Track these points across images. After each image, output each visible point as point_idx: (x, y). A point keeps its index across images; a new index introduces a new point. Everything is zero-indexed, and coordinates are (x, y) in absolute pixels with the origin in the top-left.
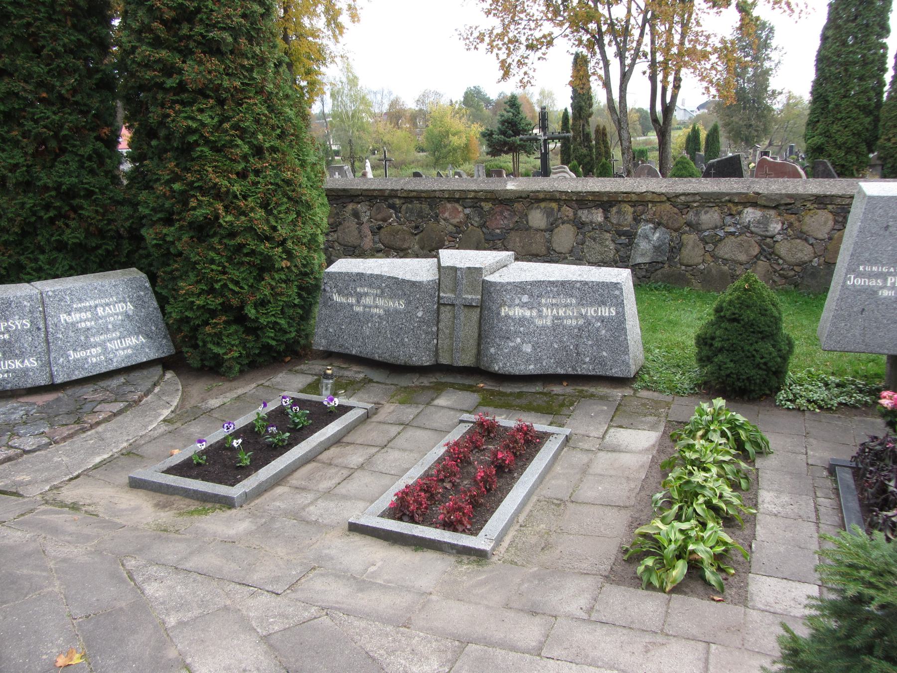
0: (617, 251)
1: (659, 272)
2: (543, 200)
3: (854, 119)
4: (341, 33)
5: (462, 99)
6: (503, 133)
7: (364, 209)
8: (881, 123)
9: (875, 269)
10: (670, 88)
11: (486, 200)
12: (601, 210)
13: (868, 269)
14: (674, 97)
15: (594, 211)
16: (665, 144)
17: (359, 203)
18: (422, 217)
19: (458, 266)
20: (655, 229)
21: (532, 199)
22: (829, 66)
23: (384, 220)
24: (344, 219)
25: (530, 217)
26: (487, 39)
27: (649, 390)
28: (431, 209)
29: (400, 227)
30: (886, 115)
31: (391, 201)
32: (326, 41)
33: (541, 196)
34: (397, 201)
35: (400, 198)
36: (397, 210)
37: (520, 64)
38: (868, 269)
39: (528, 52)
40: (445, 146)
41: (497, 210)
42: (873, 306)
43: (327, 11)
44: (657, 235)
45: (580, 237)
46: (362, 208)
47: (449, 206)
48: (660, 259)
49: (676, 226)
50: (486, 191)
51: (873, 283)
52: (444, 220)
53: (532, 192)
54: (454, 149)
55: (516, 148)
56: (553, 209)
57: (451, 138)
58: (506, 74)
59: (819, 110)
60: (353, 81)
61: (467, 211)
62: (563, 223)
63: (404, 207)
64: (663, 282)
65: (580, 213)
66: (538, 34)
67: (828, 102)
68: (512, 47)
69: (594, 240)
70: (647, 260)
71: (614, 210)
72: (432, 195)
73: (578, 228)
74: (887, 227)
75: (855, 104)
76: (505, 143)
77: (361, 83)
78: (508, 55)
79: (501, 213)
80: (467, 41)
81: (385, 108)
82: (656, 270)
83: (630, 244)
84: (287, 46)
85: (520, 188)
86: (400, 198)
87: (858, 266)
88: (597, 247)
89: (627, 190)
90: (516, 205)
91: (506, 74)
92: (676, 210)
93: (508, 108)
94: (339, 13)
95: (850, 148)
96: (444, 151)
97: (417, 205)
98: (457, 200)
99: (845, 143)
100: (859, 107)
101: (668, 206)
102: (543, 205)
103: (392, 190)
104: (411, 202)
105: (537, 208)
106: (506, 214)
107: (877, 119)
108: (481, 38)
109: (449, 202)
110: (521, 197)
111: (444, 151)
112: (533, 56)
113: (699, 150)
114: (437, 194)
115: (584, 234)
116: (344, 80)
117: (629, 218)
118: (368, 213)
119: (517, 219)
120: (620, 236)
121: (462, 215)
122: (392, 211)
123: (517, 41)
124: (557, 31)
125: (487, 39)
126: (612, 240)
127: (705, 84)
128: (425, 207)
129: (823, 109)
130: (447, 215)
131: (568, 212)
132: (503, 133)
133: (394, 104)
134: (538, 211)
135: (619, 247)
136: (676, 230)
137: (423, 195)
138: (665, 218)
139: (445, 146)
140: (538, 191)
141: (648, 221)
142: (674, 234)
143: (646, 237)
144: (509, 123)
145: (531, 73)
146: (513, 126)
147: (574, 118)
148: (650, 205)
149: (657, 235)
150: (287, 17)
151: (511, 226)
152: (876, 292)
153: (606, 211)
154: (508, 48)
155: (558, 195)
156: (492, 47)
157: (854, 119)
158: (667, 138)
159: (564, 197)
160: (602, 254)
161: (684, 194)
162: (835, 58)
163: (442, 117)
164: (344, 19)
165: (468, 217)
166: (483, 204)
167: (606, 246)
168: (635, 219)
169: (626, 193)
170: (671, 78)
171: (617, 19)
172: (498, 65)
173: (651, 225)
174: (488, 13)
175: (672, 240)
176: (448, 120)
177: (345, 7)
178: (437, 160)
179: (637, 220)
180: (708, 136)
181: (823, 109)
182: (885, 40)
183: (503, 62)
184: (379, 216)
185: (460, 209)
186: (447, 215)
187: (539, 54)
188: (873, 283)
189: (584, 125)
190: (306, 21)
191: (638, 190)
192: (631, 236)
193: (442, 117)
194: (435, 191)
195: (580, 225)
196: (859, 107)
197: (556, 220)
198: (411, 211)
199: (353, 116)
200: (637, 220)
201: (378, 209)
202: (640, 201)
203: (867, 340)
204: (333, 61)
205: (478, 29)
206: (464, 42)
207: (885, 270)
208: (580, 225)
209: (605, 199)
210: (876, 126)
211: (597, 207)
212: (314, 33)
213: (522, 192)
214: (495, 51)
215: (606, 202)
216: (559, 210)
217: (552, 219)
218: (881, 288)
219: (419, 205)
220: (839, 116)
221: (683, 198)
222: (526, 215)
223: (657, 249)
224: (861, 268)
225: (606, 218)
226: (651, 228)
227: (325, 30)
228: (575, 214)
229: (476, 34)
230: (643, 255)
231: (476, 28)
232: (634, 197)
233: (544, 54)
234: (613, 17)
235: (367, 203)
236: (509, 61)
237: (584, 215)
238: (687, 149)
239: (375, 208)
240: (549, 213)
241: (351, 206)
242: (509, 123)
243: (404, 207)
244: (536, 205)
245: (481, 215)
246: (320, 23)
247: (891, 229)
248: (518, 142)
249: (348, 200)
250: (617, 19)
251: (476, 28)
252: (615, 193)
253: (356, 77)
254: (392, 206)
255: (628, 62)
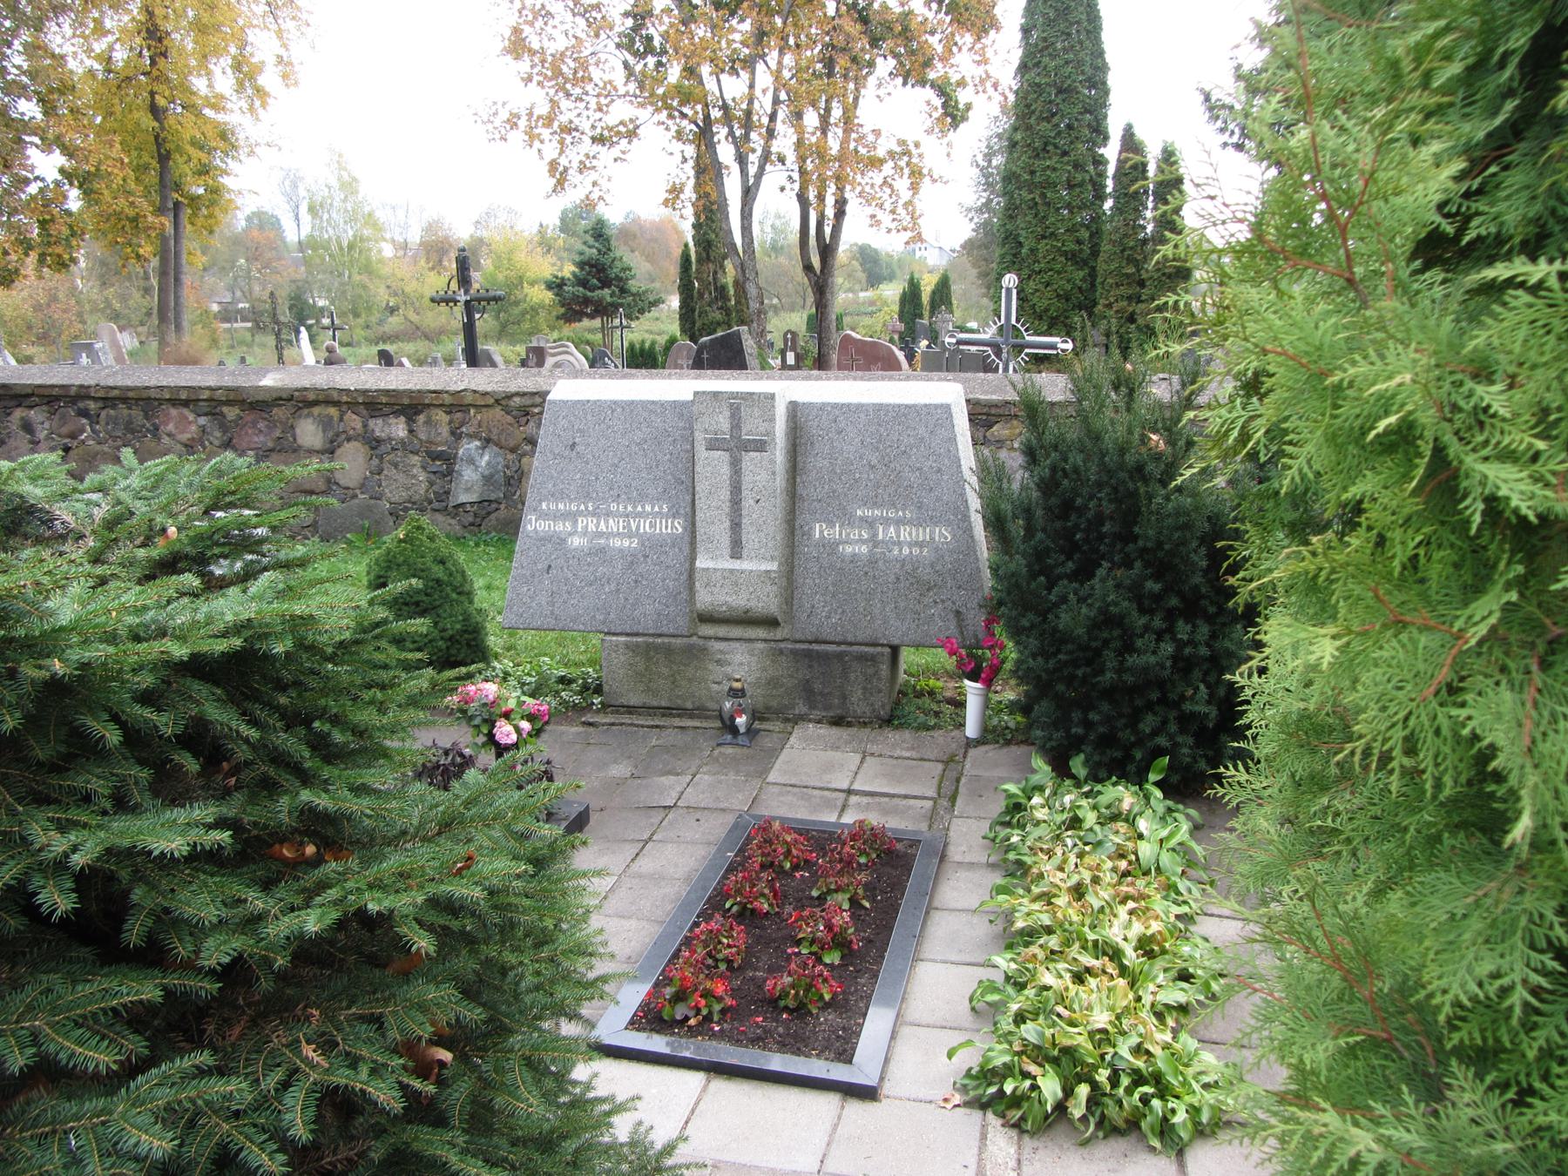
0: (432, 484)
1: (493, 516)
2: (316, 403)
3: (1059, 273)
4: (264, 105)
5: (558, 223)
6: (582, 283)
7: (40, 418)
8: (1099, 280)
9: (561, 506)
10: (830, 212)
11: (229, 403)
12: (402, 419)
13: (553, 507)
14: (837, 229)
15: (392, 420)
16: (826, 306)
17: (31, 407)
18: (133, 431)
19: (728, 524)
20: (484, 448)
21: (301, 401)
22: (1020, 188)
23: (73, 436)
24: (9, 435)
25: (298, 431)
26: (523, 123)
27: (849, 725)
28: (147, 417)
29: (98, 447)
30: (1105, 267)
31: (81, 405)
32: (235, 116)
33: (311, 397)
34: (92, 405)
35: (94, 399)
36: (94, 419)
37: (583, 168)
38: (553, 507)
39: (597, 148)
40: (517, 303)
41: (249, 418)
42: (561, 561)
43: (237, 66)
44: (486, 458)
45: (375, 462)
46: (36, 415)
47: (174, 412)
48: (493, 497)
49: (512, 443)
50: (228, 389)
51: (560, 527)
52: (169, 435)
53: (297, 390)
54: (532, 308)
55: (605, 308)
56: (331, 418)
57: (527, 288)
58: (561, 183)
59: (1009, 258)
60: (349, 187)
61: (202, 421)
62: (349, 440)
63: (103, 414)
64: (499, 531)
65: (372, 423)
66: (612, 119)
67: (1020, 244)
68: (569, 139)
69: (396, 466)
70: (473, 498)
71: (421, 418)
72: (145, 395)
73: (373, 448)
74: (574, 445)
75: (1059, 249)
76: (587, 301)
77: (365, 190)
78: (562, 152)
79: (254, 424)
80: (490, 127)
81: (415, 236)
82: (489, 513)
83: (449, 473)
84: (156, 124)
85: (279, 384)
86: (94, 399)
87: (540, 501)
88: (401, 477)
89: (438, 388)
90: (275, 410)
91: (561, 183)
92: (509, 419)
93: (591, 241)
94: (259, 69)
95: (1057, 318)
96: (516, 311)
97: (123, 411)
98: (186, 403)
99: (1046, 310)
100: (1065, 254)
101: (497, 412)
102: (316, 410)
103: (81, 386)
104: (114, 407)
105: (308, 416)
106: (261, 425)
107: (1093, 274)
108: (512, 122)
109: (174, 405)
110: (281, 399)
111: (516, 311)
112: (605, 154)
113: (921, 316)
114: (153, 393)
115: (381, 458)
116: (335, 183)
117: (445, 431)
118: (47, 425)
119: (278, 433)
120: (433, 460)
121: (193, 428)
122: (84, 421)
123: (576, 130)
124: (644, 114)
125: (523, 123)
126: (424, 468)
127: (870, 210)
128: (137, 414)
129: (1015, 255)
130: (171, 427)
131: (354, 421)
132: (582, 283)
133: (430, 228)
134: (310, 420)
135: (433, 477)
136: (513, 450)
137: (131, 394)
138: (495, 431)
139: (517, 303)
140: (306, 389)
141: (472, 436)
142: (510, 457)
143: (471, 461)
144: (592, 266)
145: (603, 182)
146: (599, 271)
147: (699, 261)
148: (472, 411)
149: (486, 458)
150: (155, 73)
151: (270, 444)
152: (564, 541)
153: (410, 420)
154: (562, 142)
155: (335, 395)
156: (532, 137)
157: (1059, 273)
158: (829, 296)
159: (345, 399)
160: (408, 489)
161: (517, 394)
162: (1027, 177)
163: (511, 252)
164: (269, 79)
165: (203, 429)
166: (225, 409)
167: (414, 476)
168: (453, 433)
169: (435, 392)
170: (830, 200)
171: (734, 100)
172: (544, 168)
173: (478, 443)
174: (528, 79)
175: (507, 467)
176: (521, 257)
177: (271, 60)
178: (504, 326)
179: (456, 435)
180: (934, 293)
181: (1015, 255)
182: (1101, 151)
183: (553, 165)
184: (65, 430)
185: (191, 417)
186: (171, 427)
187: (616, 152)
188: (560, 527)
189: (715, 273)
190: (199, 84)
191: (453, 388)
192: (449, 459)
193: (511, 252)
194: (147, 388)
195: (374, 443)
196: (1065, 254)
197: (337, 435)
198: (115, 421)
199: (351, 247)
200: (456, 435)
201: (63, 417)
202: (457, 404)
203: (557, 612)
204: (251, 153)
205: (508, 107)
206: (485, 127)
207: (574, 508)
208: (374, 443)
209: (406, 401)
210: (1093, 285)
211: (396, 413)
212: (218, 103)
213: (281, 389)
214: (537, 144)
215: (410, 406)
216: (341, 420)
217: (330, 434)
218: (570, 534)
219: (126, 412)
220: (1037, 267)
221: (517, 399)
222: (292, 427)
223: (488, 479)
224: (544, 506)
225: (411, 431)
226: (477, 448)
227: (234, 98)
228: (365, 426)
229: (504, 115)
230: (468, 490)
231: (504, 104)
232: (448, 399)
233: (623, 152)
234: (726, 96)
235: (45, 408)
236: (563, 161)
237: (378, 427)
238: (901, 318)
239: (57, 417)
240: (326, 423)
241: (18, 414)
242: (592, 266)
243: (103, 414)
244: (306, 411)
245: (224, 427)
246: (224, 81)
247: (578, 448)
248: (609, 299)
249: (13, 403)
250: (734, 100)
251: (504, 104)
252: (419, 391)
253: (355, 179)
254: (84, 413)
255: (752, 170)
